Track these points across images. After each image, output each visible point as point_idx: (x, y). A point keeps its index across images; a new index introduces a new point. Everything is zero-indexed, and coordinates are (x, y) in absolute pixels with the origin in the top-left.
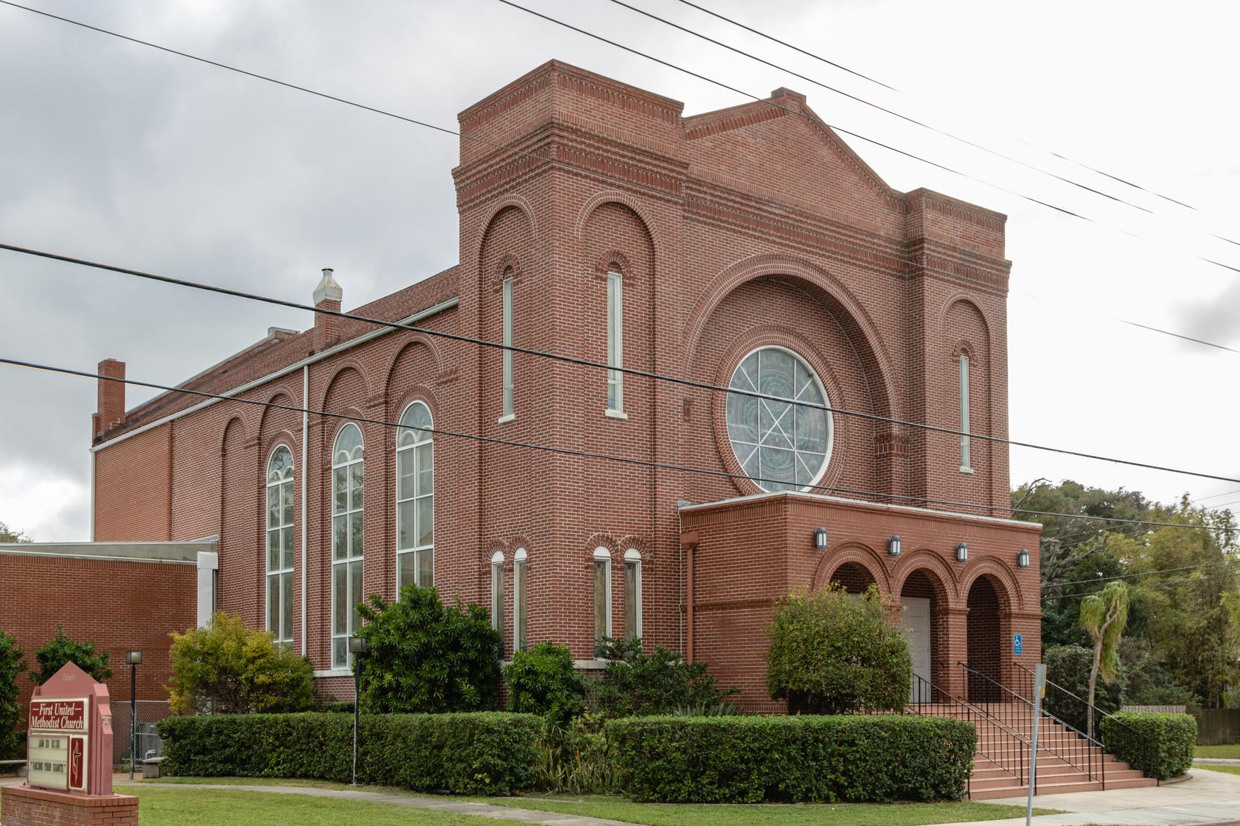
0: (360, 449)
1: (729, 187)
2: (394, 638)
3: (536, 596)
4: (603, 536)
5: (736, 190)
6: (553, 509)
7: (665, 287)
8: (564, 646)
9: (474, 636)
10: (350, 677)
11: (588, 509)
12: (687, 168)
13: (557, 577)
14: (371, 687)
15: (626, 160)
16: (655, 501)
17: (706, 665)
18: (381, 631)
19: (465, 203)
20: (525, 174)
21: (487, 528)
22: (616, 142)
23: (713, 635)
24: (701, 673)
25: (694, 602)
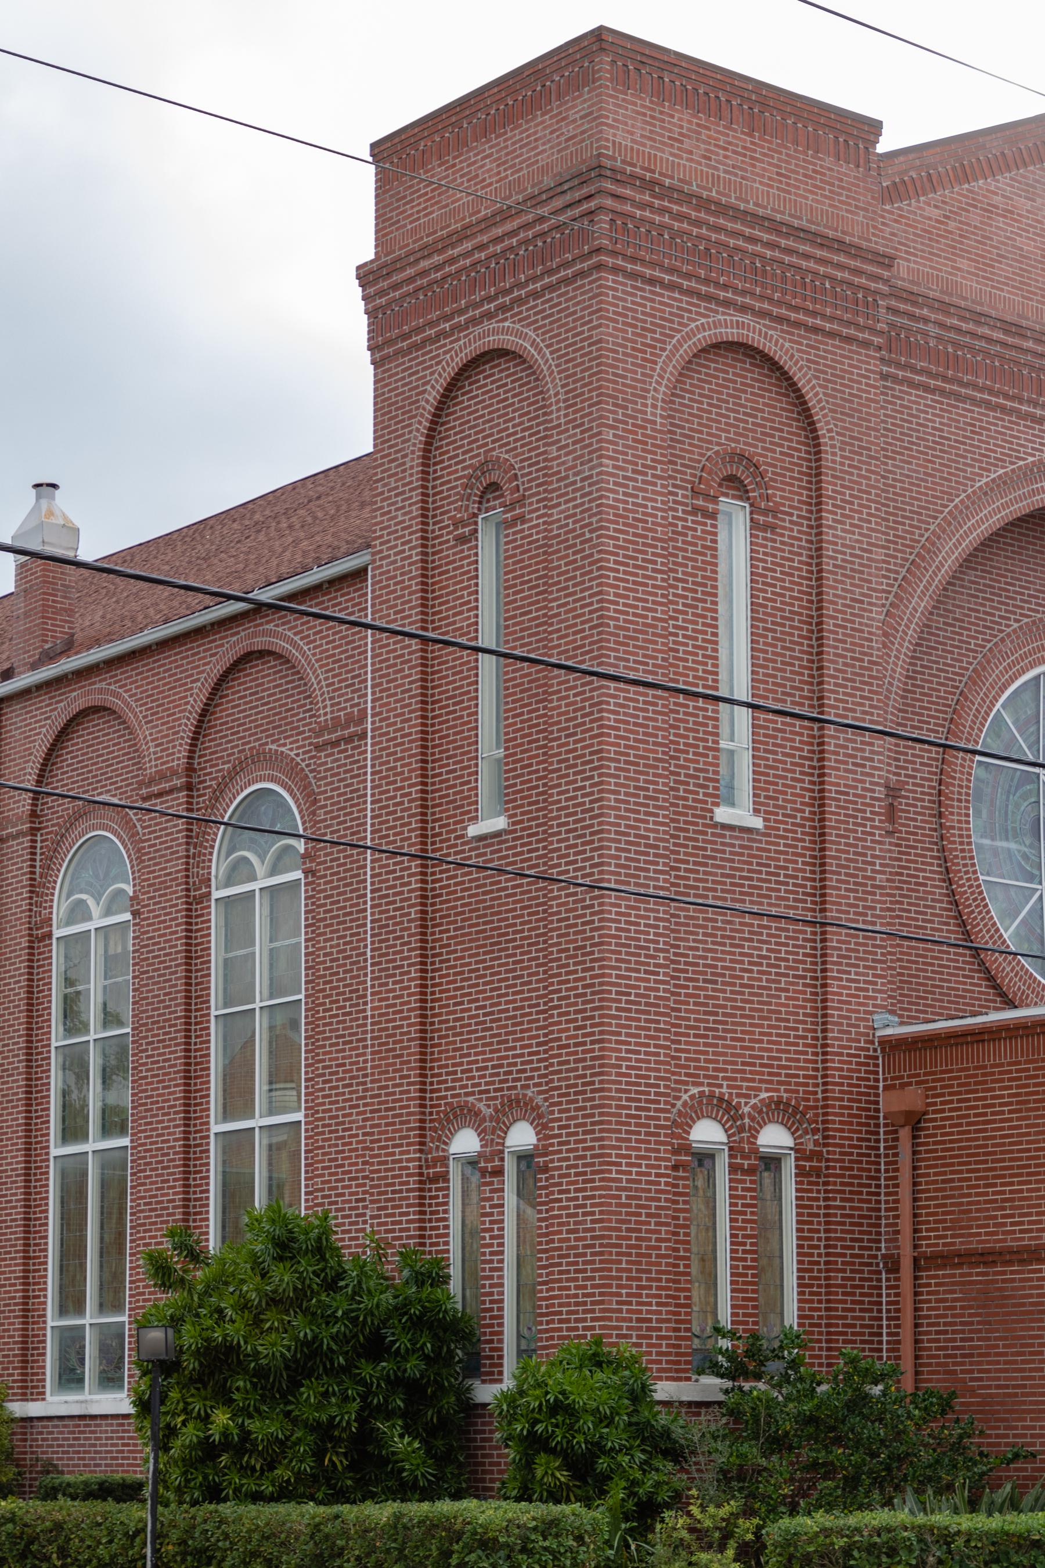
0: (122, 891)
1: (979, 309)
2: (235, 1330)
3: (560, 1232)
4: (712, 1095)
5: (993, 313)
6: (601, 1033)
7: (844, 530)
8: (626, 1347)
9: (418, 1323)
10: (126, 1416)
11: (676, 1034)
12: (890, 266)
13: (610, 1188)
14: (179, 1443)
15: (758, 248)
16: (825, 1016)
17: (953, 1395)
18: (203, 1311)
19: (389, 342)
20: (534, 279)
21: (440, 1075)
22: (736, 209)
23: (962, 1323)
24: (943, 1412)
25: (915, 1247)
